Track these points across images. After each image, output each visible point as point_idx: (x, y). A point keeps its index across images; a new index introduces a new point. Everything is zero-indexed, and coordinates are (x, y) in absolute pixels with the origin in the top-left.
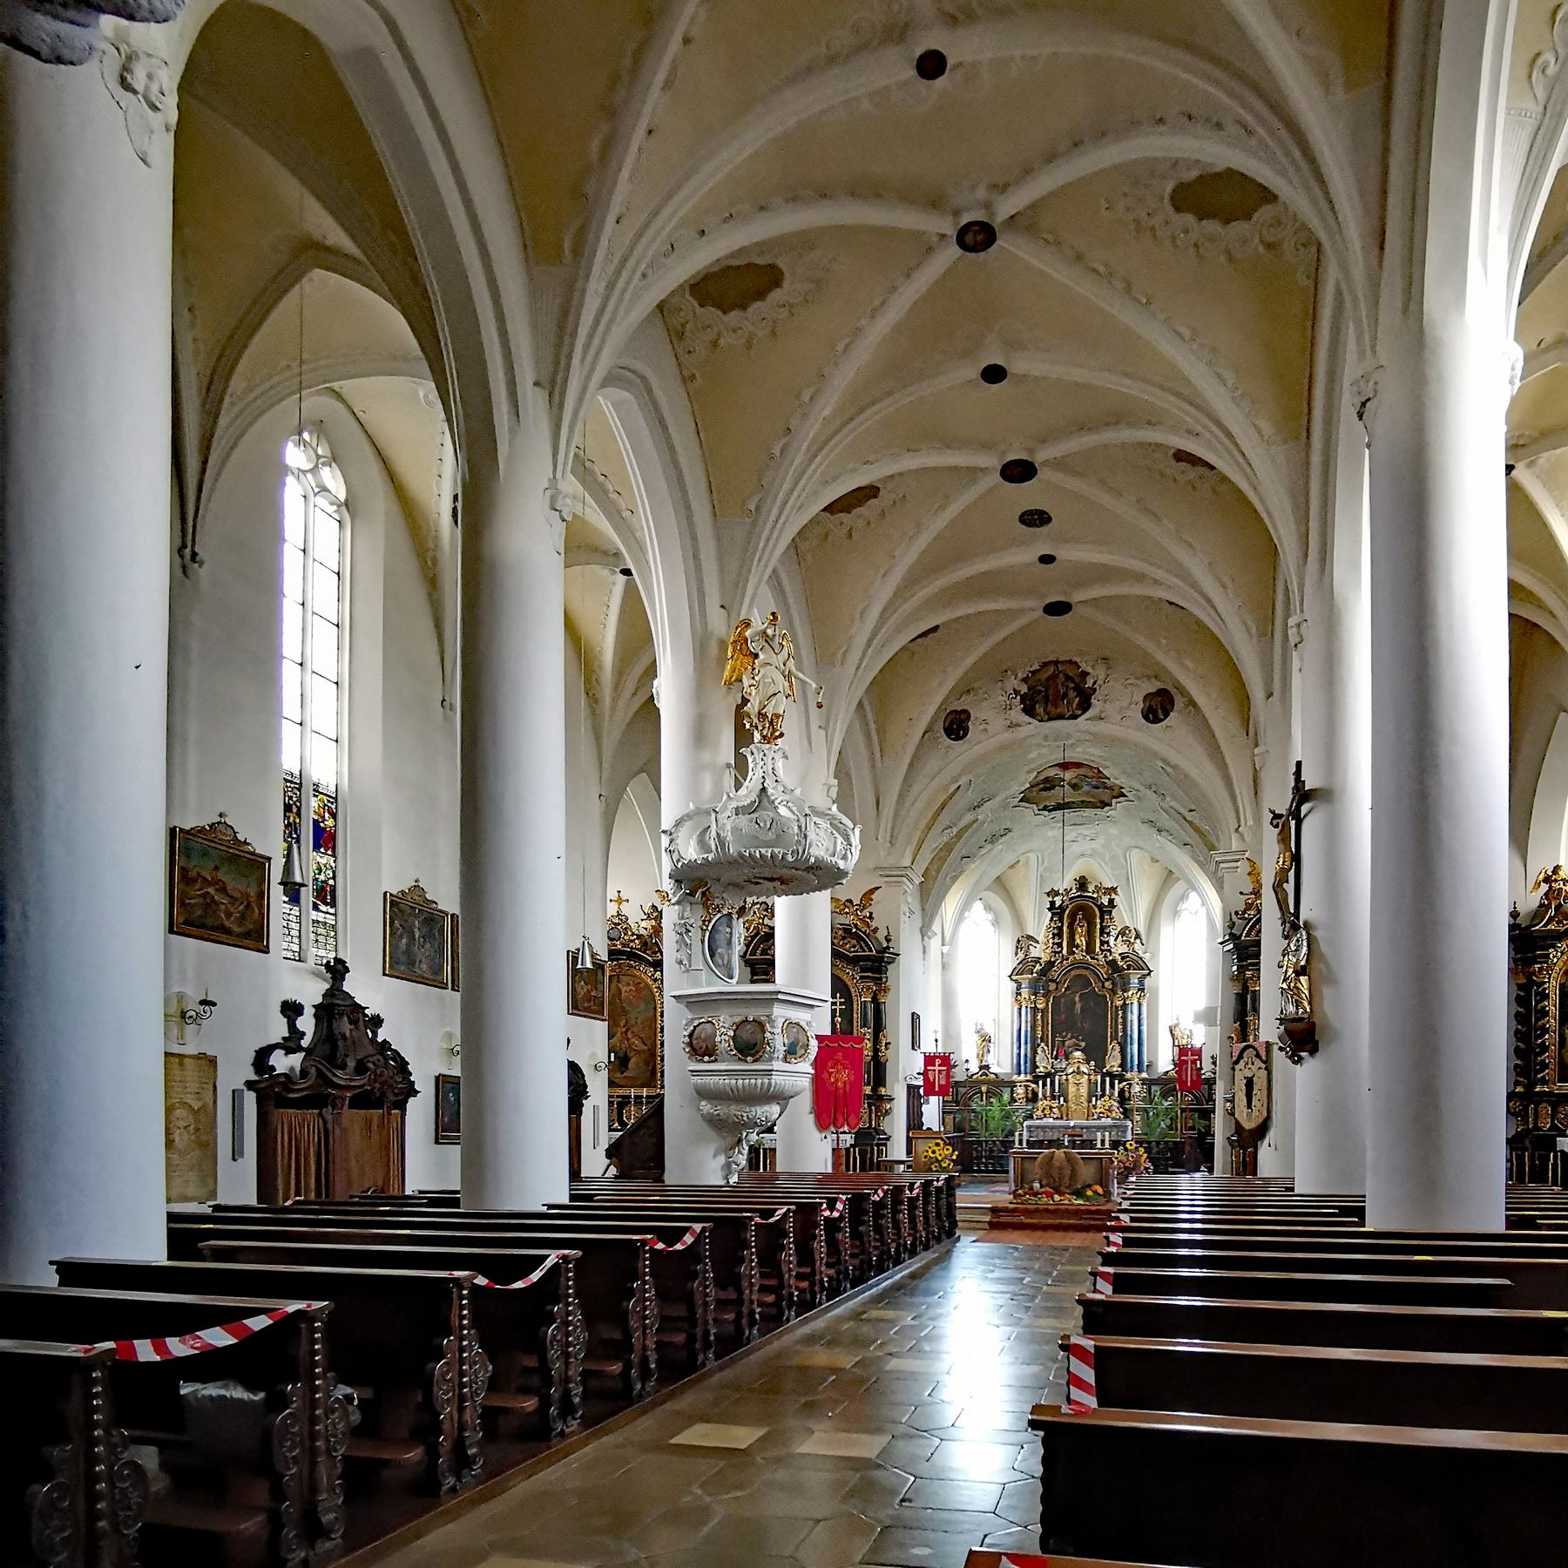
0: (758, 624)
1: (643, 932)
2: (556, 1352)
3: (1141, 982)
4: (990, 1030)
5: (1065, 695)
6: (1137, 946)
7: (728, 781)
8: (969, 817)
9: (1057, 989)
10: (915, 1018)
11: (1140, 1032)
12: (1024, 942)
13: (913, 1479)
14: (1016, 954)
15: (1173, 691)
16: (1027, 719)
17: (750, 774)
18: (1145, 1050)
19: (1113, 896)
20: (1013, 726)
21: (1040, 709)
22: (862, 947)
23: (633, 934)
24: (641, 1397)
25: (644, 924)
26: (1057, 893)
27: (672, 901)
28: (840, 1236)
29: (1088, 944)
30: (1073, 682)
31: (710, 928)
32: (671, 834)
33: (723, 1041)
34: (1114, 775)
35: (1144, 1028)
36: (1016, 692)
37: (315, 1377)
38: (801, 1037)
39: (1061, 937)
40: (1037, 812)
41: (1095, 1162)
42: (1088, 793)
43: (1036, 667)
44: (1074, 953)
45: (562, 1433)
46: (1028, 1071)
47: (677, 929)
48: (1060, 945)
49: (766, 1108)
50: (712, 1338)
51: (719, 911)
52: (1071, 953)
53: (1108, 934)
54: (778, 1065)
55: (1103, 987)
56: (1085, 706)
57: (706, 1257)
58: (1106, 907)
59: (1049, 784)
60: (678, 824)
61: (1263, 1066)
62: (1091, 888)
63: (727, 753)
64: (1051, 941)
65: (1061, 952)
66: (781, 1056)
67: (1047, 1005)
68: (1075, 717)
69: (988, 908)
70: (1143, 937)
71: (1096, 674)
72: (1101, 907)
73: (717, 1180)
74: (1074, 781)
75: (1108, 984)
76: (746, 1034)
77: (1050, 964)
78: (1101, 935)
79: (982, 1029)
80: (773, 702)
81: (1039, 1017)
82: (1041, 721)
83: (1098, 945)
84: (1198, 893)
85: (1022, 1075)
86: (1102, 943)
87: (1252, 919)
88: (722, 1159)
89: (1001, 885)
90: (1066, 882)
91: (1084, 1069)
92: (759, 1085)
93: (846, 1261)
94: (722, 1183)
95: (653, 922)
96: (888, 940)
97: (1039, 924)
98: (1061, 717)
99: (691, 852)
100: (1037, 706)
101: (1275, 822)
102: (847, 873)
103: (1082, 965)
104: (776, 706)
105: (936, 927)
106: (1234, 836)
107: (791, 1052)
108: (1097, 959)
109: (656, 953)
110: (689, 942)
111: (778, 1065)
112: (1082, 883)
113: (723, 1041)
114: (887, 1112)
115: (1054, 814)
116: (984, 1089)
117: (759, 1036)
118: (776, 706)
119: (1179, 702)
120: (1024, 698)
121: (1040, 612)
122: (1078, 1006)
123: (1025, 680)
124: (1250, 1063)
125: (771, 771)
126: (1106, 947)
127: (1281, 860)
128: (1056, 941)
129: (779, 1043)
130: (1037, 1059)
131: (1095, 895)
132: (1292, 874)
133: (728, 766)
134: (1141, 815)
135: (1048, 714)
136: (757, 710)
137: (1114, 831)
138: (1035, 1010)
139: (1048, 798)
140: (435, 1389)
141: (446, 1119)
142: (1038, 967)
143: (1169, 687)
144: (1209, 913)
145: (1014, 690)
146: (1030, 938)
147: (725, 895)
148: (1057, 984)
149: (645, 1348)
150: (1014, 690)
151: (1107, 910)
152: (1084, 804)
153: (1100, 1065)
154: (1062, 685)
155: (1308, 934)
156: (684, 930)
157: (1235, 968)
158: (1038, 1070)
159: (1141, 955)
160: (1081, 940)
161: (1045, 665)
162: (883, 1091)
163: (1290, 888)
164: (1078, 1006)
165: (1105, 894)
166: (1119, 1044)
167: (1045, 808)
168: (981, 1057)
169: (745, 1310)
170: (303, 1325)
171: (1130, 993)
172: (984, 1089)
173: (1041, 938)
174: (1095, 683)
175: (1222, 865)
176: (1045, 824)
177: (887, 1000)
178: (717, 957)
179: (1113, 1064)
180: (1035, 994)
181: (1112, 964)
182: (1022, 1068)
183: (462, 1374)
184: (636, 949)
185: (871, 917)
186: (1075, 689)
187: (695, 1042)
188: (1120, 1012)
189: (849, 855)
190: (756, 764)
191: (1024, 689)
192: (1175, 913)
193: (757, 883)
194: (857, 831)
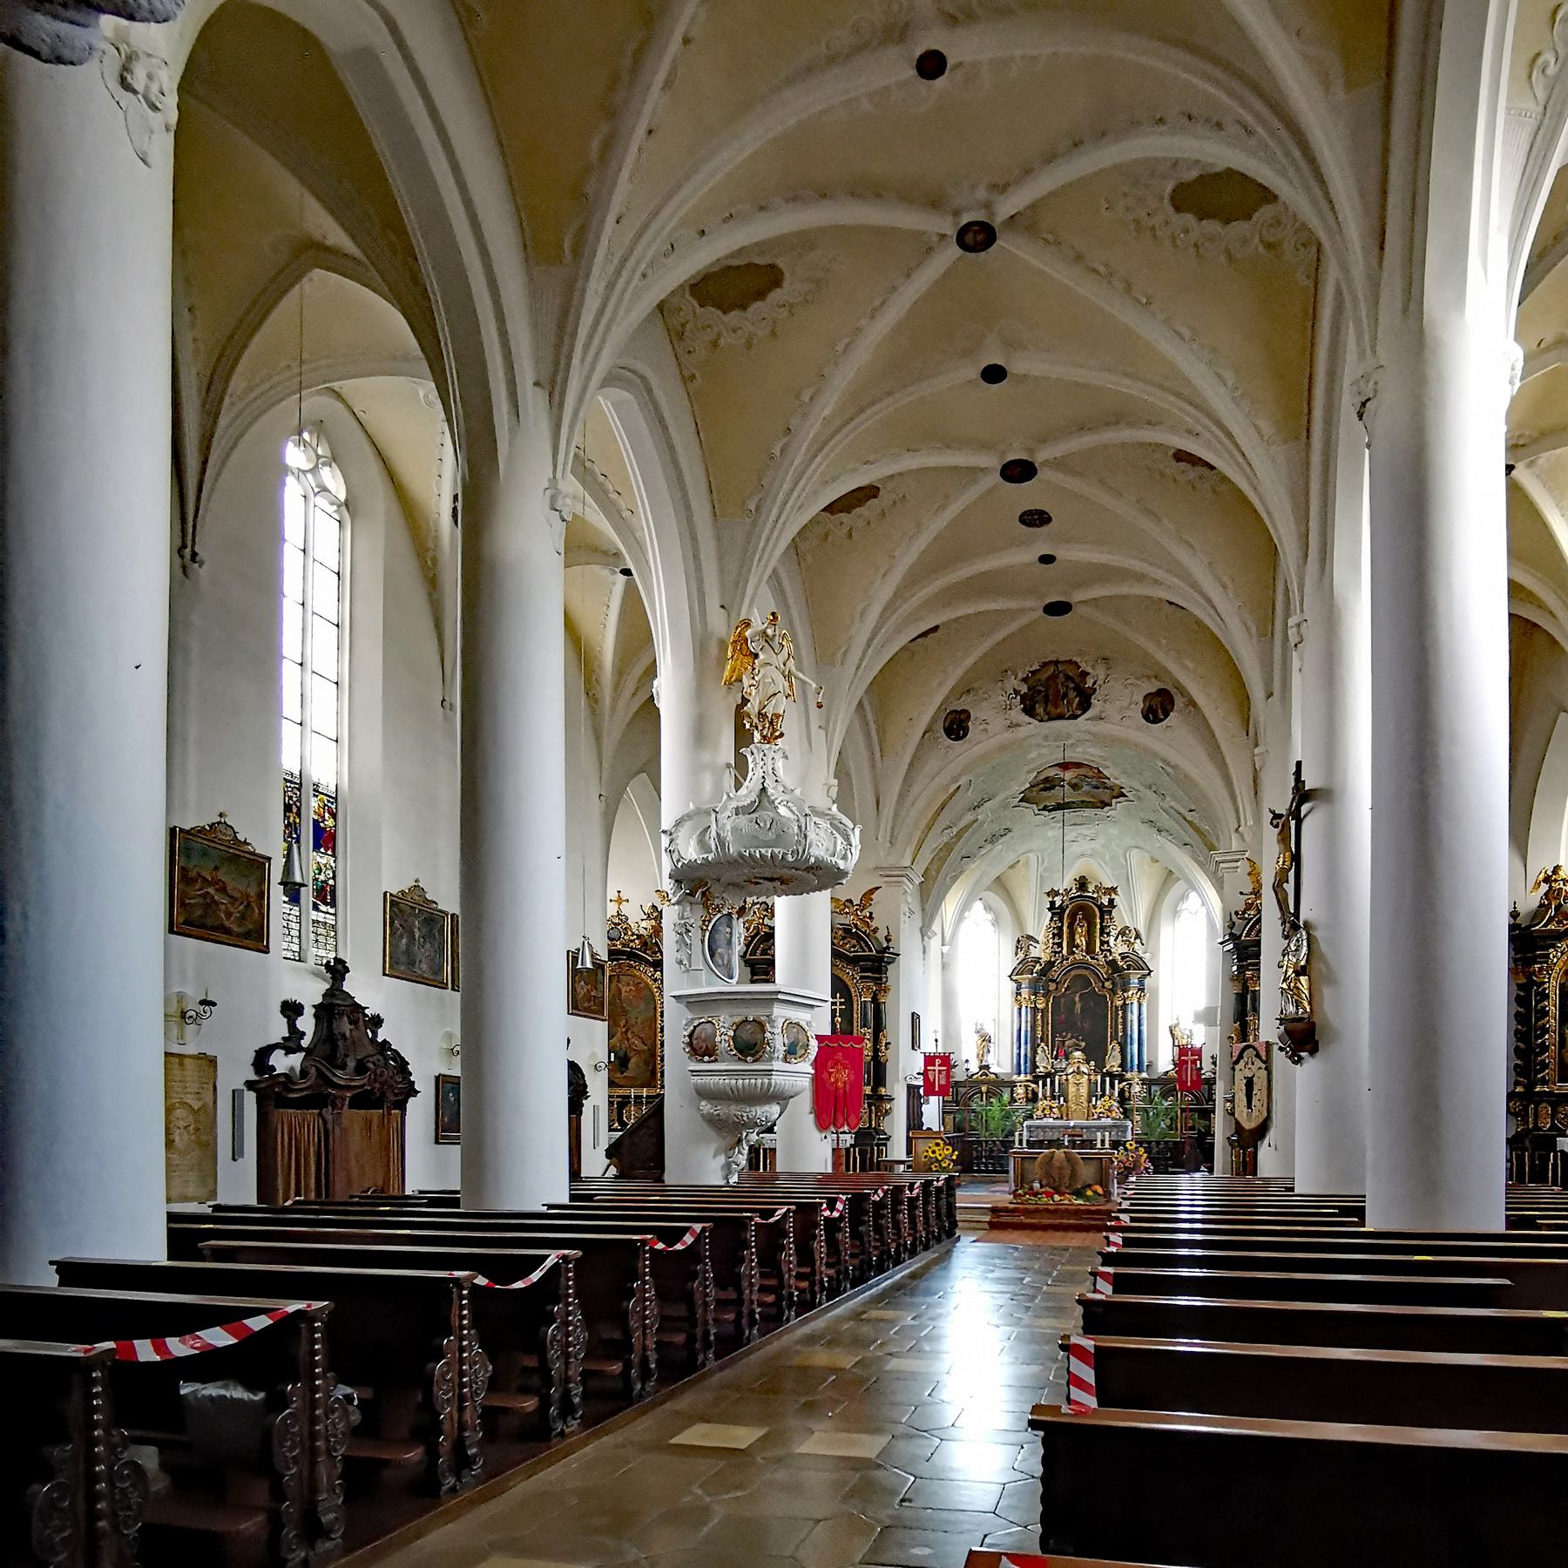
0: (758, 624)
1: (643, 932)
2: (556, 1352)
3: (1141, 982)
4: (990, 1030)
5: (1065, 695)
6: (1137, 946)
7: (728, 781)
8: (969, 817)
9: (1057, 989)
10: (915, 1018)
11: (1140, 1032)
12: (1024, 942)
13: (913, 1479)
14: (1016, 954)
15: (1173, 691)
16: (1027, 719)
17: (750, 774)
18: (1145, 1050)
19: (1113, 896)
20: (1013, 726)
21: (1040, 709)
22: (862, 947)
23: (633, 934)
24: (641, 1397)
25: (644, 924)
26: (1057, 893)
27: (672, 901)
28: (840, 1236)
29: (1088, 944)
30: (1073, 682)
31: (710, 928)
32: (671, 834)
33: (723, 1041)
34: (1114, 775)
35: (1144, 1028)
36: (1016, 692)
37: (315, 1377)
38: (801, 1037)
39: (1061, 937)
40: (1037, 812)
41: (1095, 1162)
42: (1088, 793)
43: (1036, 667)
44: (1074, 953)
45: (562, 1433)
46: (1028, 1071)
47: (677, 929)
48: (1060, 945)
49: (766, 1108)
50: (712, 1338)
51: (719, 911)
52: (1071, 953)
53: (1108, 934)
54: (778, 1065)
55: (1103, 987)
56: (1085, 706)
57: (706, 1257)
58: (1106, 907)
59: (1049, 784)
60: (678, 824)
61: (1263, 1066)
62: (1091, 888)
63: (727, 753)
64: (1051, 941)
65: (1061, 952)
66: (781, 1056)
67: (1047, 1005)
68: (1075, 717)
69: (988, 908)
70: (1143, 937)
71: (1096, 674)
72: (1101, 907)
73: (717, 1180)
74: (1074, 781)
75: (1108, 984)
76: (746, 1034)
77: (1050, 964)
78: (1101, 935)
79: (982, 1029)
80: (773, 702)
81: (1039, 1017)
82: (1041, 721)
83: (1098, 945)
84: (1198, 893)
85: (1022, 1075)
86: (1102, 943)
87: (1252, 919)
88: (722, 1159)
89: (1001, 885)
90: (1066, 882)
91: (1084, 1069)
92: (759, 1085)
93: (846, 1261)
94: (722, 1183)
95: (653, 922)
96: (888, 940)
97: (1039, 924)
98: (1061, 717)
99: (691, 852)
100: (1037, 706)
101: (1275, 822)
102: (847, 873)
103: (1082, 965)
104: (776, 706)
105: (936, 927)
106: (1234, 836)
107: (791, 1052)
108: (1097, 959)
109: (656, 953)
110: (689, 942)
111: (778, 1065)
112: (1082, 883)
113: (723, 1041)
114: (887, 1112)
115: (1054, 814)
116: (984, 1089)
117: (759, 1036)
118: (776, 706)
119: (1179, 702)
120: (1024, 698)
121: (1040, 612)
122: (1078, 1006)
123: (1025, 680)
124: (1250, 1063)
125: (771, 771)
126: (1106, 947)
127: (1281, 860)
128: (1056, 941)
129: (779, 1043)
130: (1037, 1059)
131: (1095, 895)
132: (1292, 874)
133: (728, 766)
134: (1141, 815)
135: (1048, 714)
136: (757, 710)
137: (1114, 831)
138: (1035, 1010)
139: (1048, 798)
140: (435, 1389)
141: (446, 1119)
142: (1038, 967)
143: (1169, 687)
144: (1209, 913)
145: (1014, 690)
146: (1030, 938)
147: (725, 895)
148: (1057, 984)
149: (645, 1348)
150: (1014, 690)
151: (1107, 910)
152: (1084, 804)
153: (1100, 1065)
154: (1062, 685)
155: (1308, 934)
156: (684, 930)
157: (1235, 968)
158: (1038, 1070)
159: (1141, 955)
160: (1081, 940)
161: (1045, 665)
162: (883, 1091)
163: (1290, 888)
164: (1078, 1006)
165: (1105, 894)
166: (1119, 1044)
167: (1045, 808)
168: (981, 1057)
169: (745, 1310)
170: (303, 1325)
171: (1130, 993)
172: (984, 1089)
173: (1041, 938)
174: (1095, 683)
175: (1222, 865)
176: (1045, 824)
177: (887, 1000)
178: (717, 957)
179: (1113, 1064)
180: (1035, 994)
181: (1112, 964)
182: (1022, 1068)
183: (462, 1374)
184: (636, 949)
185: (871, 917)
186: (1075, 689)
187: (695, 1042)
188: (1120, 1012)
189: (849, 855)
190: (756, 764)
191: (1024, 689)
192: (1175, 913)
193: (757, 883)
194: (857, 831)
